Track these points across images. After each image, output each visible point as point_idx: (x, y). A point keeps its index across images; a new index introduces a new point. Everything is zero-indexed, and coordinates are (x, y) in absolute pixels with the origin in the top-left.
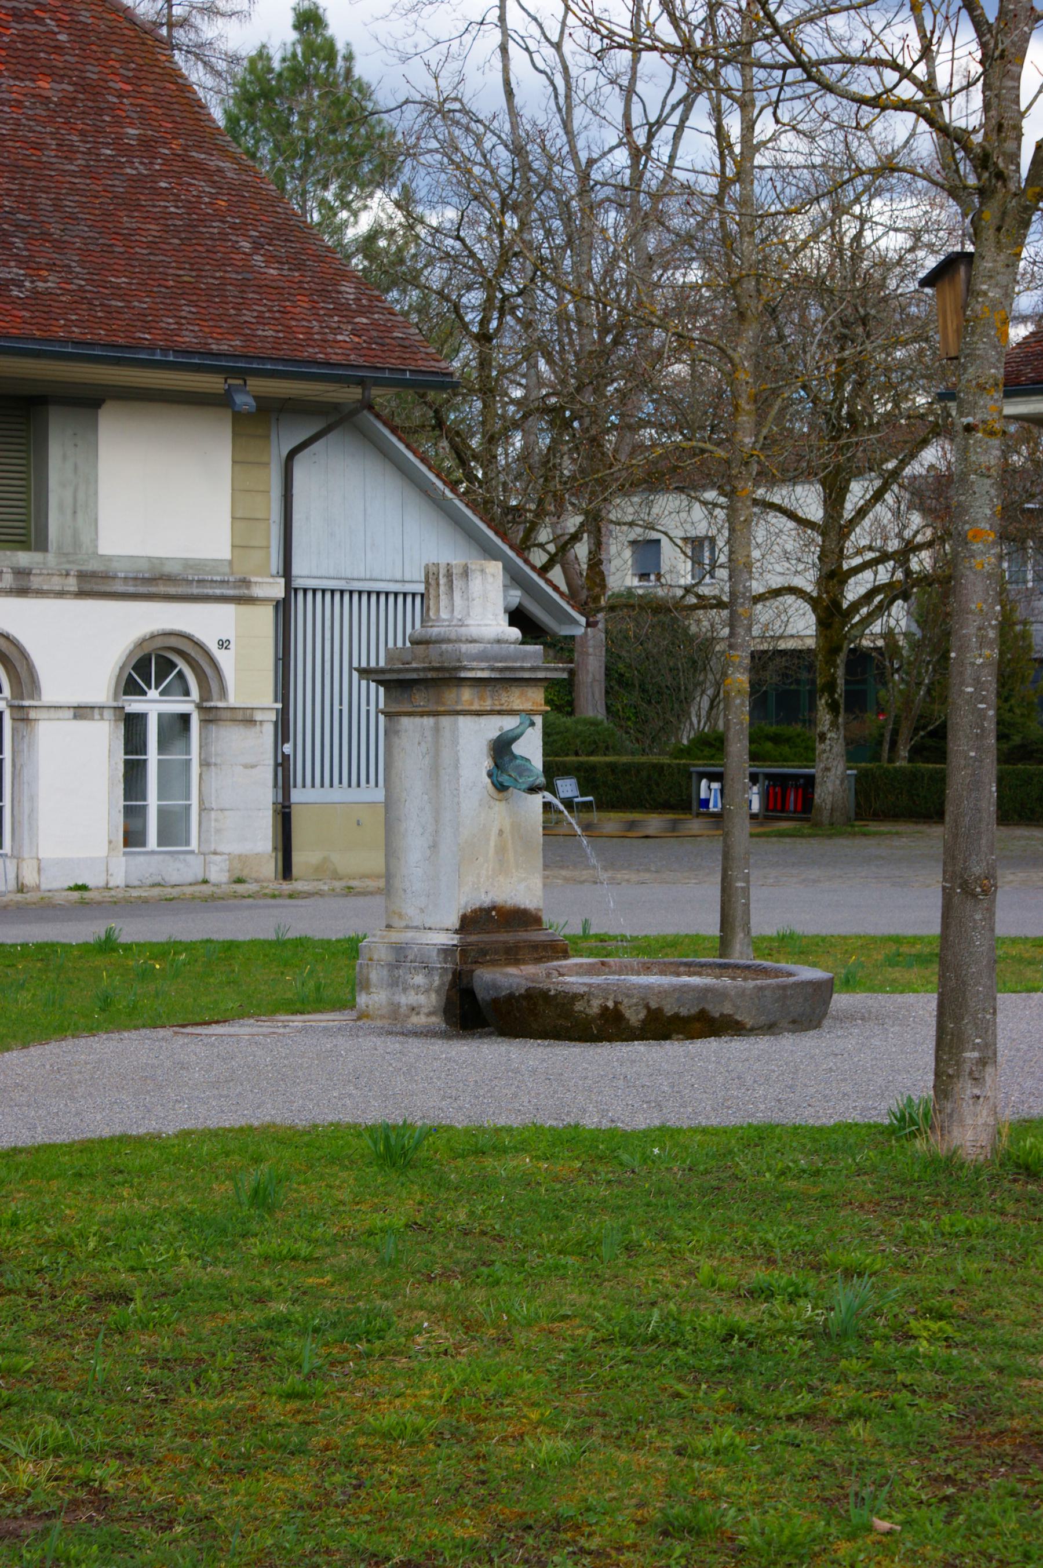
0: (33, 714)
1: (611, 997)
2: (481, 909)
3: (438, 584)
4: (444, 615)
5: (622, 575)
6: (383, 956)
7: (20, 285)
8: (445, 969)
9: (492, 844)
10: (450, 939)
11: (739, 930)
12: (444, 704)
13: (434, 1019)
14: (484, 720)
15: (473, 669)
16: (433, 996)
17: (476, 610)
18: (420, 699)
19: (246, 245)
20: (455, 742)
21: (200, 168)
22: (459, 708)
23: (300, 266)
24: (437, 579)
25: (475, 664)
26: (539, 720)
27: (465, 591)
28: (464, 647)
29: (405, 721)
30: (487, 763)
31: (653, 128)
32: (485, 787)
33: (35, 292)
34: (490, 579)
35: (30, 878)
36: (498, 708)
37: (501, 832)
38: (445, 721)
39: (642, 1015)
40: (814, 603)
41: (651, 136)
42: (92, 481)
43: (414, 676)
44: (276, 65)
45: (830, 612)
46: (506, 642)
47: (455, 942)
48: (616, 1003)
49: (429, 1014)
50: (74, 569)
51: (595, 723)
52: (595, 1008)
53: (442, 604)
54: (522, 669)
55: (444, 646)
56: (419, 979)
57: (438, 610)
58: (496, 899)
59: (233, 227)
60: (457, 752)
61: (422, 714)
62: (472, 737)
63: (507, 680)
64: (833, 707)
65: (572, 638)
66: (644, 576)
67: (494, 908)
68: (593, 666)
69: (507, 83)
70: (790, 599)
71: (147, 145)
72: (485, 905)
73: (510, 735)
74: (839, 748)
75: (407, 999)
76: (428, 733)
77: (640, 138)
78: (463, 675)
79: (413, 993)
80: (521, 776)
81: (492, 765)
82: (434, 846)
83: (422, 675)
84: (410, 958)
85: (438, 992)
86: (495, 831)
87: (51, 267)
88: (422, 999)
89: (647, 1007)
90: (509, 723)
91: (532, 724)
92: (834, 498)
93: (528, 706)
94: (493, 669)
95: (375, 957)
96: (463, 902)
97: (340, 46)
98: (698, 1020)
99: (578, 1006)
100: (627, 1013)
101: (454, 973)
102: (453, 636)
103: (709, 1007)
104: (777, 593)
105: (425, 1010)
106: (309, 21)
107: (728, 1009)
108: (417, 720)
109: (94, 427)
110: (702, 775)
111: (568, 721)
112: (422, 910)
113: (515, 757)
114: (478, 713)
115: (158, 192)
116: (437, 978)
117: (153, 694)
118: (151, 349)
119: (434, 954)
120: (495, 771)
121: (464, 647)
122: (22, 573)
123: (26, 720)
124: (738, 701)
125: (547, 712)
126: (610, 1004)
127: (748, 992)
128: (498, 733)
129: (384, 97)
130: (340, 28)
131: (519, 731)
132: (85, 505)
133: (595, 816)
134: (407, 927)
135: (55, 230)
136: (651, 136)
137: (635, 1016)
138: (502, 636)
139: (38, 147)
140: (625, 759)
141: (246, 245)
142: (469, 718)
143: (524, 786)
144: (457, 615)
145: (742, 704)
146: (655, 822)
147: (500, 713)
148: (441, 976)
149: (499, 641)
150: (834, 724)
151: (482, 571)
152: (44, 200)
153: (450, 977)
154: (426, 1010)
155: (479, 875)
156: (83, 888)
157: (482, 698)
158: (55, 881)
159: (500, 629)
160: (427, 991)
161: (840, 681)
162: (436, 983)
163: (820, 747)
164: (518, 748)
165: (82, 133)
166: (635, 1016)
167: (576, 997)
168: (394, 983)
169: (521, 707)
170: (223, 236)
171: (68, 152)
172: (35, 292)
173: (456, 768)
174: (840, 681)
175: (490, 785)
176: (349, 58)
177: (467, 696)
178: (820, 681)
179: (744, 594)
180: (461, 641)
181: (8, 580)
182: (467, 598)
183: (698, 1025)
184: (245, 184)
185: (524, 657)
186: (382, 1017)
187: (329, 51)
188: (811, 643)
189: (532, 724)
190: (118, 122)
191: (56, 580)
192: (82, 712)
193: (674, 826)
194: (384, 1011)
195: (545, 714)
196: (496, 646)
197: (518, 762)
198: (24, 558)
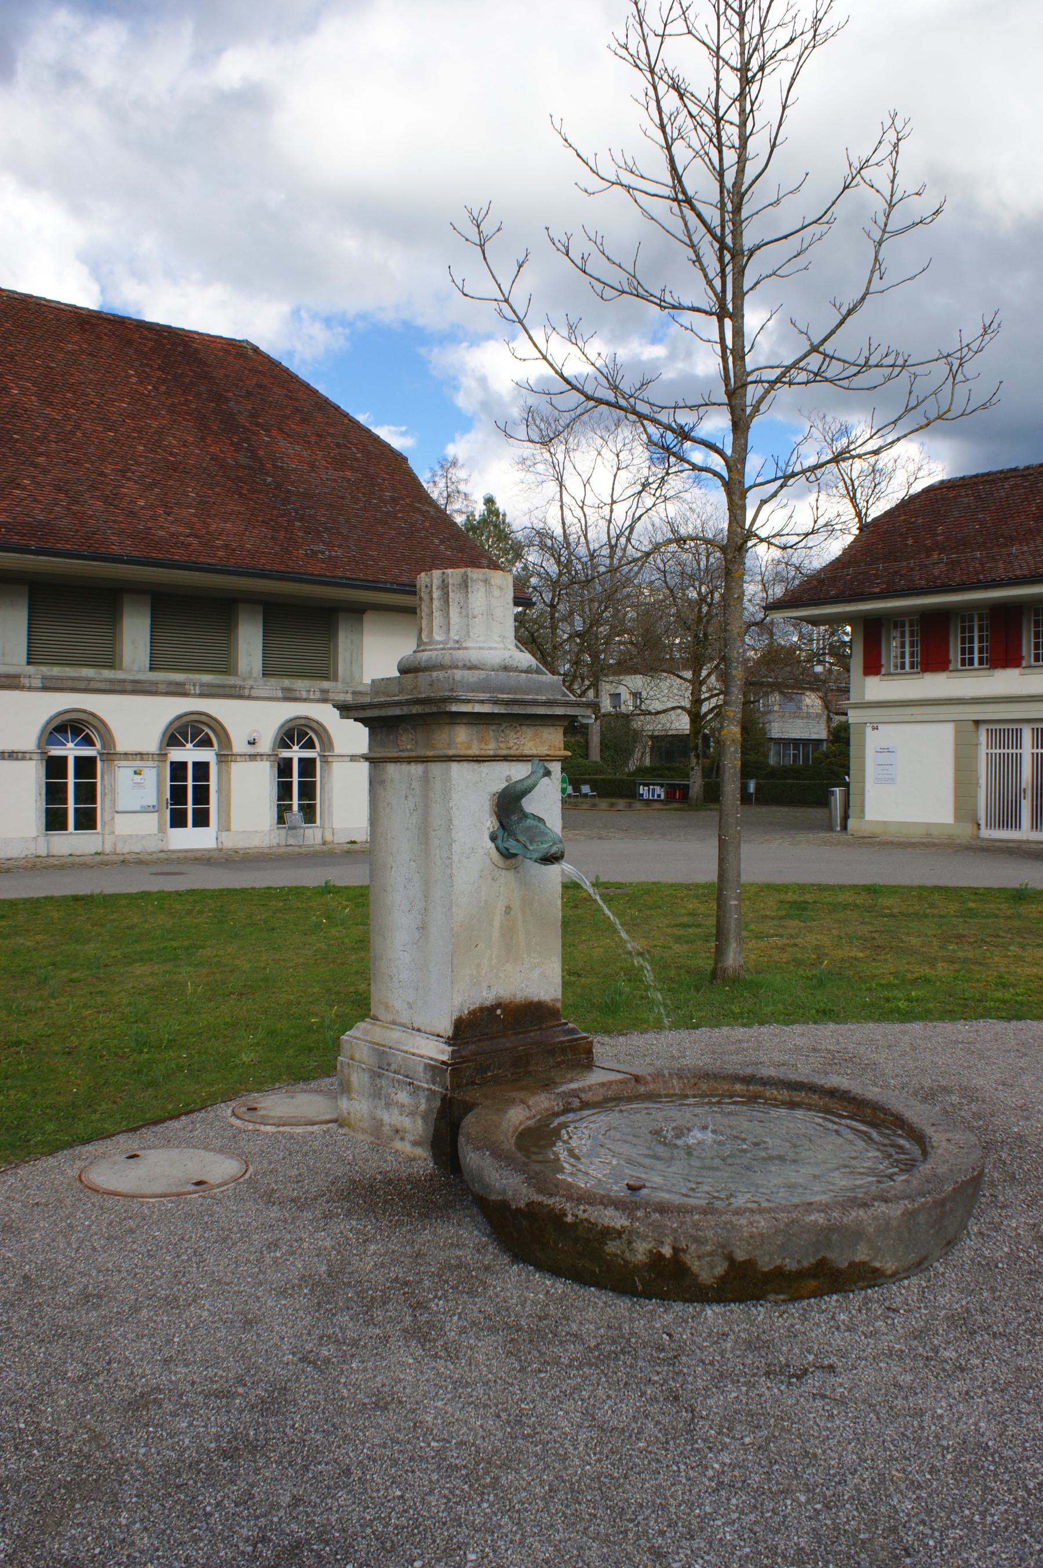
0: (330, 759)
1: (668, 1240)
2: (482, 1009)
3: (431, 599)
4: (438, 637)
5: (606, 705)
6: (365, 1058)
7: (323, 553)
8: (433, 1092)
9: (497, 924)
10: (441, 1052)
11: (732, 941)
12: (434, 748)
13: (419, 1151)
14: (485, 768)
15: (469, 701)
16: (420, 1122)
17: (478, 628)
18: (407, 742)
19: (437, 541)
20: (447, 796)
21: (419, 510)
22: (451, 752)
23: (462, 551)
24: (431, 592)
25: (470, 695)
26: (556, 768)
27: (463, 607)
28: (458, 674)
29: (392, 769)
30: (489, 823)
31: (618, 537)
32: (488, 854)
33: (330, 556)
34: (496, 593)
35: (328, 837)
36: (504, 752)
37: (508, 909)
38: (435, 768)
39: (720, 1270)
40: (689, 713)
41: (618, 540)
42: (360, 648)
43: (397, 711)
44: (477, 518)
45: (696, 717)
46: (516, 669)
47: (445, 1058)
48: (676, 1250)
49: (415, 1144)
50: (350, 690)
51: (596, 762)
52: (641, 1249)
53: (436, 623)
54: (535, 703)
55: (435, 674)
56: (403, 1097)
57: (431, 631)
58: (502, 993)
59: (432, 534)
60: (449, 811)
61: (410, 760)
62: (469, 792)
63: (512, 717)
64: (697, 756)
65: (587, 724)
66: (615, 707)
67: (499, 1005)
68: (595, 740)
69: (563, 519)
70: (679, 711)
71: (394, 500)
72: (488, 1003)
73: (520, 787)
74: (699, 773)
75: (391, 1118)
76: (416, 785)
77: (613, 542)
78: (455, 708)
79: (396, 1111)
80: (532, 842)
81: (497, 825)
82: (423, 928)
83: (406, 710)
84: (393, 1067)
85: (425, 1118)
86: (500, 907)
87: (340, 546)
88: (406, 1122)
89: (730, 1258)
90: (519, 772)
91: (548, 773)
92: (697, 673)
93: (543, 750)
94: (496, 702)
95: (357, 1057)
96: (457, 1003)
97: (501, 511)
98: (815, 1276)
99: (612, 1247)
100: (695, 1266)
101: (444, 1099)
102: (447, 661)
103: (832, 1255)
104: (674, 708)
105: (410, 1137)
106: (489, 501)
107: (862, 1254)
108: (405, 767)
109: (361, 621)
110: (641, 784)
111: (586, 762)
112: (410, 1006)
113: (525, 816)
114: (478, 759)
115: (398, 519)
116: (423, 1101)
117: (296, 748)
118: (385, 582)
119: (421, 1068)
120: (500, 833)
121: (458, 674)
122: (324, 691)
123: (327, 762)
124: (732, 749)
125: (566, 757)
126: (667, 1251)
127: (894, 1223)
128: (505, 785)
129: (515, 527)
130: (501, 505)
131: (530, 781)
132: (357, 659)
133: (597, 800)
134: (394, 1023)
135: (345, 532)
136: (618, 540)
137: (707, 1270)
138: (509, 662)
139: (342, 498)
140: (609, 777)
141: (437, 541)
142: (465, 765)
143: (536, 856)
144: (454, 635)
145: (736, 752)
146: (621, 803)
147: (506, 758)
148: (428, 1100)
149: (506, 668)
150: (697, 763)
151: (486, 581)
152: (341, 519)
153: (439, 1104)
154: (412, 1138)
155: (479, 966)
156: (354, 842)
157: (482, 740)
158: (341, 838)
159: (507, 654)
160: (412, 1114)
161: (700, 745)
162: (423, 1107)
163: (692, 773)
164: (530, 805)
165: (364, 493)
166: (707, 1270)
167: (608, 1233)
168: (376, 1094)
169: (534, 752)
170: (427, 537)
171: (355, 500)
172: (330, 556)
173: (449, 830)
174: (700, 745)
175: (494, 853)
176: (504, 515)
177: (462, 737)
178: (692, 745)
179: (737, 659)
180: (457, 667)
181: (318, 695)
182: (466, 614)
183: (813, 1284)
184: (439, 518)
185: (540, 688)
186: (364, 1131)
187: (497, 514)
188: (688, 732)
189: (548, 773)
190: (381, 490)
191: (342, 695)
192: (353, 758)
193: (630, 805)
194: (366, 1125)
195: (564, 760)
196: (502, 675)
197: (530, 822)
198: (326, 685)
